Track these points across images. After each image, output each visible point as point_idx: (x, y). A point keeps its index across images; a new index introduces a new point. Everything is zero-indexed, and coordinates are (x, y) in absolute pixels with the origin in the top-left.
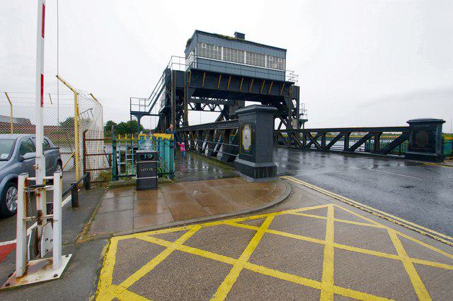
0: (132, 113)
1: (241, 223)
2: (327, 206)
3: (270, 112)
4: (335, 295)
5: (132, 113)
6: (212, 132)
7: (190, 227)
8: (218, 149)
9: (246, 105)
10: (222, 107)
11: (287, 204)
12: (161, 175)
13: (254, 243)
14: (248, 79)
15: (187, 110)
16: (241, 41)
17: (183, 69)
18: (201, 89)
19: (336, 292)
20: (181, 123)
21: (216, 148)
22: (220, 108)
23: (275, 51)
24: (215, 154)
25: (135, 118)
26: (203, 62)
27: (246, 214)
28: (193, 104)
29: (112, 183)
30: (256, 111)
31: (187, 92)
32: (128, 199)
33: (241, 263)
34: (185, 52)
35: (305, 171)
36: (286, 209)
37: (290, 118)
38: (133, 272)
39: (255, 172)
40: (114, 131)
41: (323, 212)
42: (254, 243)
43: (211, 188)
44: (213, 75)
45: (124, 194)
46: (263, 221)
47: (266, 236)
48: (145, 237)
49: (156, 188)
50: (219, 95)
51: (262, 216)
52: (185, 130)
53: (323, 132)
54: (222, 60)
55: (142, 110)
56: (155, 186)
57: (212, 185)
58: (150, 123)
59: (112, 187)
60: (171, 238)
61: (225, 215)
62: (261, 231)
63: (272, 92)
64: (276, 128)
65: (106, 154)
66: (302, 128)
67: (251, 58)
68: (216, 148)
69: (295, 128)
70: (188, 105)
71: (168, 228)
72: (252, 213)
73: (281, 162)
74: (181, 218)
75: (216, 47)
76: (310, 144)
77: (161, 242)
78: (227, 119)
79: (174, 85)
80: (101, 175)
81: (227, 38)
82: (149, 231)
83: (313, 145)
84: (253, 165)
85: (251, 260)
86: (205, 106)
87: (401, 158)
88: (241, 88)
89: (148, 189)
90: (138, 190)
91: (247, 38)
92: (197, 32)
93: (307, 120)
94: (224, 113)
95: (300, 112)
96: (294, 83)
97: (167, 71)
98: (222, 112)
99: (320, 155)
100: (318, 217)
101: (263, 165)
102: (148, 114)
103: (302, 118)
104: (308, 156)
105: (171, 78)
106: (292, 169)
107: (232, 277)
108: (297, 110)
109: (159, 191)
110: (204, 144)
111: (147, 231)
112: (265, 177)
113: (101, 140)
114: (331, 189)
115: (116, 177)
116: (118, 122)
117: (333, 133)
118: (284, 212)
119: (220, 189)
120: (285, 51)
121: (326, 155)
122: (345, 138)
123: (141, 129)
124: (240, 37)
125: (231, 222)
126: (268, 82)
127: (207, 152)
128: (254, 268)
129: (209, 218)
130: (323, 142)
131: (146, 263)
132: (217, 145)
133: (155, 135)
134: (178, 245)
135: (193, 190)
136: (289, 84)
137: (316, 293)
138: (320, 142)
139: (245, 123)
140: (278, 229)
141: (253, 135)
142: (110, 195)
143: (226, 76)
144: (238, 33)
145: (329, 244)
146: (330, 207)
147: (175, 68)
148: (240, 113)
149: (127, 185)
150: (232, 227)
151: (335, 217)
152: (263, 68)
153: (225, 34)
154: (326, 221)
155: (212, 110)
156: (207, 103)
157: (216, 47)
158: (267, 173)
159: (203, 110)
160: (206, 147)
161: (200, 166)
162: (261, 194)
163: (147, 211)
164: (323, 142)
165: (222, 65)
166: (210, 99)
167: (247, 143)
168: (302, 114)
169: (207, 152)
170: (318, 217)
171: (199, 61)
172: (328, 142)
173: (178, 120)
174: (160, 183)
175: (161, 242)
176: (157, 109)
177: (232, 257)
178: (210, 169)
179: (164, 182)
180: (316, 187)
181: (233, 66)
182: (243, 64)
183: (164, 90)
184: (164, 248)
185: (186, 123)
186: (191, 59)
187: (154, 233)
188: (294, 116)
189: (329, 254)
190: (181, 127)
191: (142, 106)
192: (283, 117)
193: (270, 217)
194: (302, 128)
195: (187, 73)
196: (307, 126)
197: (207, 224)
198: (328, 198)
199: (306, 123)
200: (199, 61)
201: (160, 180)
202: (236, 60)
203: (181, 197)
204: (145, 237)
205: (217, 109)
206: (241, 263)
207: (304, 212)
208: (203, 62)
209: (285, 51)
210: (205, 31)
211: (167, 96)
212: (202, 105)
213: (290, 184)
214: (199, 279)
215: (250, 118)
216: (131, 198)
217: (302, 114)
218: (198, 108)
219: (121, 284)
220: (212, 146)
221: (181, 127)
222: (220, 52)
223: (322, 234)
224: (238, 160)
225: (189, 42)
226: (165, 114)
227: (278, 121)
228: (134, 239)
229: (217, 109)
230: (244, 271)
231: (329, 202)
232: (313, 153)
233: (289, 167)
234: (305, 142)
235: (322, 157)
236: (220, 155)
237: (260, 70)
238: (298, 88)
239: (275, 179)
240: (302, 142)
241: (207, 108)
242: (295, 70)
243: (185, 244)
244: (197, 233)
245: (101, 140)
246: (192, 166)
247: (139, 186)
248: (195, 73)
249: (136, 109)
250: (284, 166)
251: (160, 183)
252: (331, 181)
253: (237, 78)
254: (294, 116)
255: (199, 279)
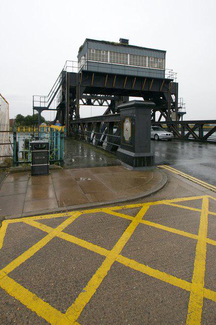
0: (35, 108)
1: (117, 211)
2: (201, 197)
3: (150, 107)
4: (205, 299)
5: (35, 108)
6: (99, 124)
7: (70, 213)
8: (104, 139)
9: (130, 100)
10: (109, 102)
11: (163, 194)
12: (52, 163)
13: (127, 235)
14: (131, 78)
15: (78, 105)
16: (125, 46)
17: (76, 71)
18: (93, 88)
19: (207, 297)
20: (73, 116)
21: (101, 139)
22: (107, 103)
23: (139, 51)
24: (101, 144)
25: (36, 112)
26: (92, 64)
27: (123, 202)
28: (84, 100)
29: (12, 168)
30: (137, 105)
31: (78, 90)
32: (25, 183)
33: (113, 255)
34: (78, 57)
35: (184, 162)
36: (161, 199)
37: (169, 111)
38: (15, 257)
39: (134, 161)
40: (21, 122)
41: (198, 204)
42: (127, 235)
43: (94, 175)
44: (100, 75)
45: (22, 178)
46: (138, 211)
47: (140, 227)
48: (31, 221)
49: (48, 174)
50: (107, 92)
51: (137, 205)
52: (77, 122)
53: (200, 124)
54: (108, 62)
55: (43, 105)
56: (46, 172)
57: (97, 172)
58: (49, 116)
59: (12, 172)
60: (54, 224)
61: (103, 203)
62: (136, 221)
63: (152, 88)
64: (157, 120)
65: (11, 144)
66: (180, 120)
67: (117, 57)
68: (101, 139)
69: (173, 120)
70: (80, 101)
71: (52, 213)
72: (129, 202)
73: (161, 152)
74: (66, 204)
75: (103, 53)
76: (188, 134)
77: (44, 228)
78: (114, 112)
79: (68, 84)
80: (6, 161)
81: (113, 44)
82: (36, 215)
83: (191, 136)
84: (132, 154)
85: (123, 253)
86: (94, 101)
87: (20, 171)
88: (125, 86)
89: (41, 174)
90: (32, 175)
91: (130, 43)
92: (88, 40)
93: (185, 113)
94: (111, 107)
95: (179, 106)
96: (173, 80)
97: (63, 73)
98: (109, 106)
99: (197, 145)
100: (192, 209)
101: (142, 155)
102: (47, 109)
103: (180, 110)
104: (185, 146)
105: (67, 79)
106: (170, 160)
107: (103, 270)
108: (176, 103)
109: (50, 177)
110: (92, 134)
111: (33, 216)
112: (144, 165)
113: (7, 132)
114: (207, 180)
115: (18, 164)
116: (25, 115)
117: (211, 125)
118: (159, 202)
119: (104, 177)
120: (165, 52)
121: (203, 145)
122: (200, 128)
123: (43, 120)
124: (124, 42)
125: (108, 211)
126: (149, 79)
127: (94, 141)
128: (126, 261)
129: (89, 205)
130: (201, 133)
131: (28, 249)
132: (103, 136)
133: (52, 126)
134: (57, 232)
135: (84, 176)
136: (168, 81)
137: (185, 295)
138: (197, 133)
139: (126, 117)
140: (152, 220)
141: (133, 127)
142: (10, 179)
143: (111, 76)
144: (122, 39)
145: (202, 239)
146: (205, 199)
147: (69, 70)
148: (122, 108)
149: (25, 171)
150: (109, 215)
151: (210, 210)
152: (146, 67)
153: (111, 40)
154: (200, 213)
155: (101, 105)
156: (97, 99)
157: (103, 53)
158: (145, 162)
159: (92, 105)
160: (93, 137)
161: (89, 155)
162: (139, 183)
163: (39, 196)
164: (201, 133)
165: (109, 66)
166: (99, 95)
167: (127, 134)
168: (181, 108)
169: (94, 141)
170: (192, 209)
171: (89, 64)
172: (205, 133)
173: (71, 113)
174: (50, 169)
175: (44, 228)
176: (55, 104)
177: (105, 248)
178: (97, 158)
179: (54, 169)
180: (192, 178)
181: (118, 67)
182: (127, 65)
183: (61, 89)
184: (45, 234)
185: (78, 116)
186: (83, 62)
187: (38, 218)
188: (173, 109)
189: (201, 250)
190: (74, 119)
191: (42, 102)
192: (163, 111)
193: (145, 207)
194: (180, 120)
195: (79, 74)
196: (185, 118)
197: (86, 212)
198: (204, 189)
199: (184, 116)
200: (89, 64)
201: (52, 166)
202: (117, 61)
203: (71, 183)
204: (31, 221)
205: (105, 103)
206: (113, 255)
207: (176, 203)
208: (92, 64)
209: (165, 52)
210: (140, 46)
211: (63, 94)
212: (92, 101)
213: (167, 173)
214: (73, 269)
215: (131, 112)
216: (25, 183)
217: (181, 108)
218: (89, 103)
219: (3, 270)
220: (98, 137)
221: (74, 119)
222: (107, 56)
223: (195, 230)
224: (120, 150)
225: (81, 49)
226: (61, 108)
227: (158, 114)
228: (22, 223)
229: (105, 103)
230: (116, 264)
231: (204, 193)
232: (191, 143)
233: (168, 157)
234: (183, 133)
235: (200, 147)
236: (105, 144)
237: (102, 66)
238: (176, 85)
239: (153, 168)
240: (180, 132)
241: (96, 103)
242: (173, 69)
243: (64, 231)
244: (76, 219)
245: (7, 132)
246: (83, 154)
247: (34, 172)
248: (85, 74)
249: (37, 105)
250: (163, 155)
251: (50, 169)
252: (207, 172)
253: (121, 77)
254: (173, 109)
255: (73, 269)
